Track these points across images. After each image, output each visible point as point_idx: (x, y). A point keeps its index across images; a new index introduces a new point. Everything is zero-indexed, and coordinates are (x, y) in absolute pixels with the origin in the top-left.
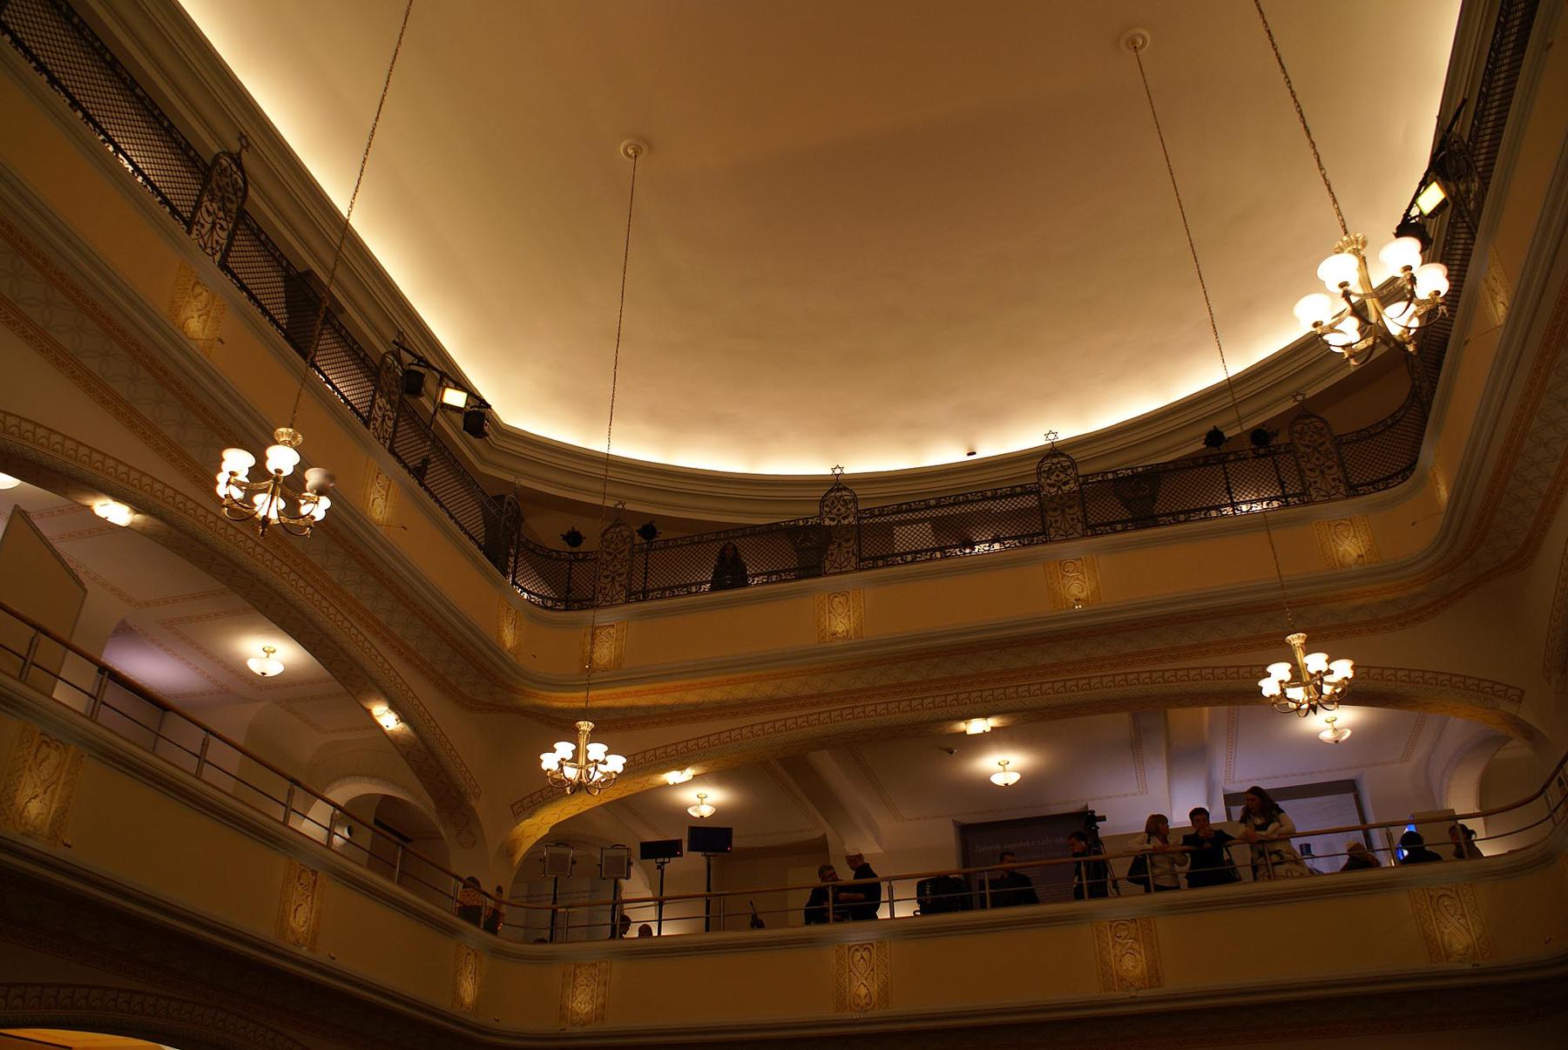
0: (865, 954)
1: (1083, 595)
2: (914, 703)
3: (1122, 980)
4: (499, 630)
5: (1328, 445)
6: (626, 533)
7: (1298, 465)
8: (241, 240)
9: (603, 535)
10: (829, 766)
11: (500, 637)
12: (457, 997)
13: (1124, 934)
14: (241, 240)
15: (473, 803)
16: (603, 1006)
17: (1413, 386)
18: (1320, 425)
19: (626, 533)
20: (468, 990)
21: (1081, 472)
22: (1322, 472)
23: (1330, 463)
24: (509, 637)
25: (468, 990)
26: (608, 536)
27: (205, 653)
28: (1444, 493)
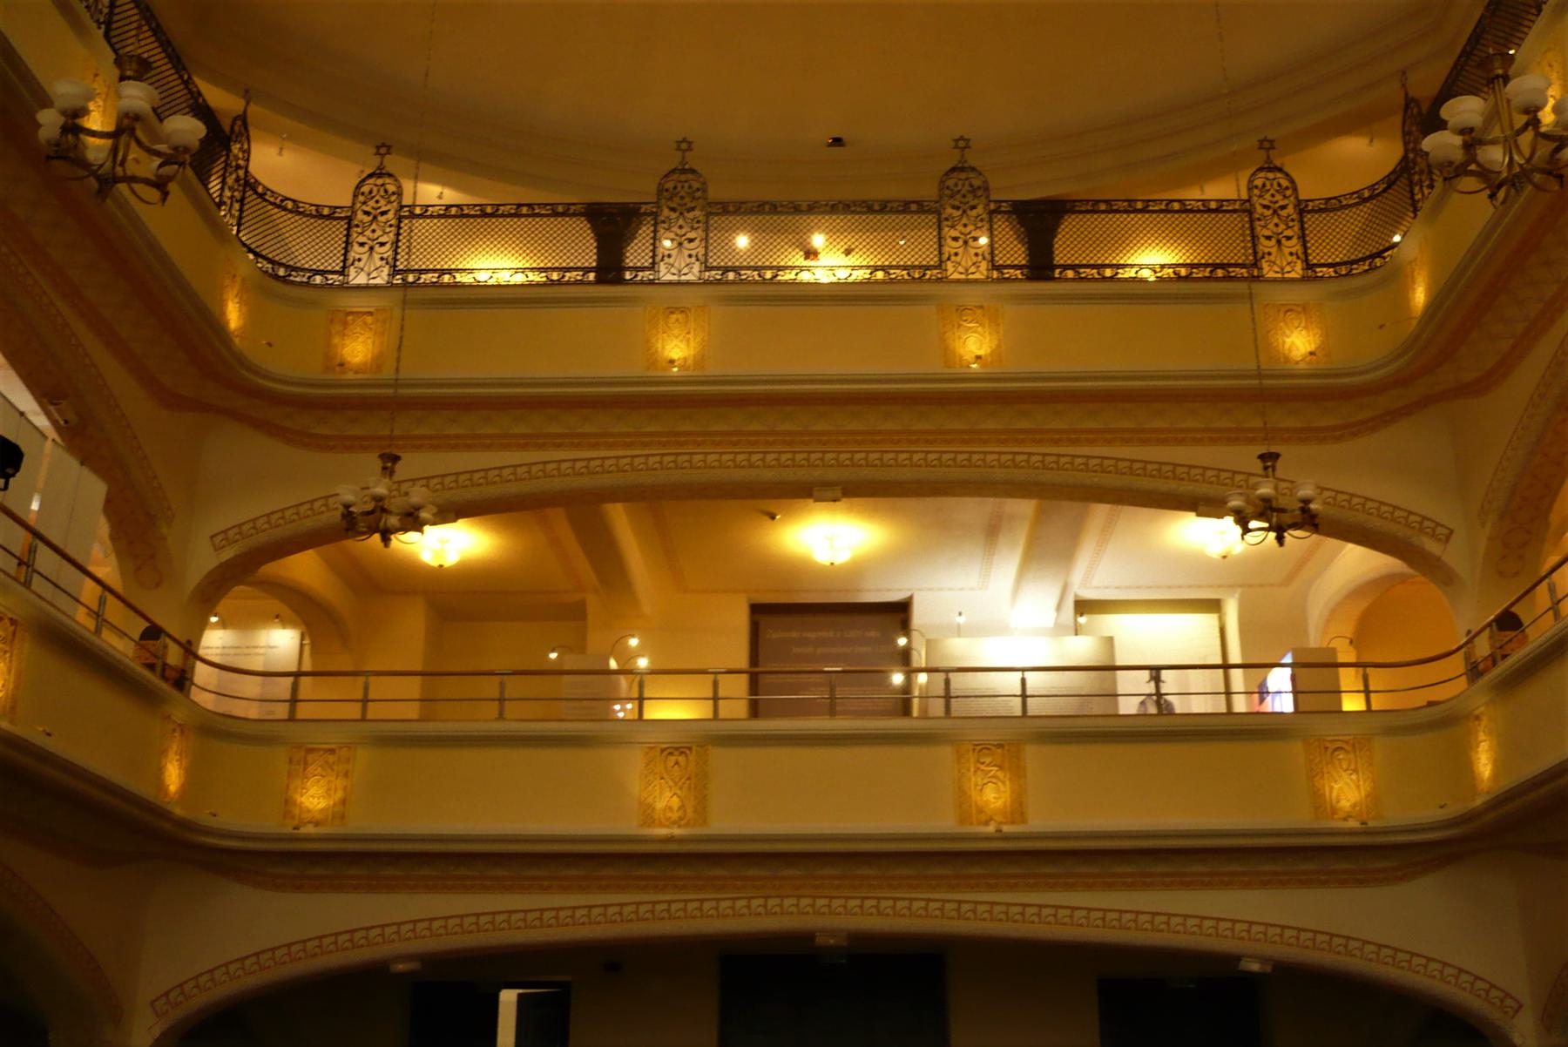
0: (681, 759)
1: (981, 352)
2: (755, 458)
3: (981, 811)
4: (222, 305)
5: (1290, 209)
6: (391, 188)
7: (1252, 229)
8: (1551, 613)
9: (358, 187)
10: (619, 517)
11: (223, 314)
12: (161, 785)
13: (988, 760)
14: (1551, 613)
15: (164, 530)
16: (344, 802)
17: (1405, 158)
18: (1285, 183)
19: (391, 188)
20: (173, 776)
21: (993, 197)
22: (1279, 242)
23: (1288, 233)
24: (234, 315)
25: (173, 776)
26: (365, 189)
27: (1021, 804)
28: (1420, 296)
